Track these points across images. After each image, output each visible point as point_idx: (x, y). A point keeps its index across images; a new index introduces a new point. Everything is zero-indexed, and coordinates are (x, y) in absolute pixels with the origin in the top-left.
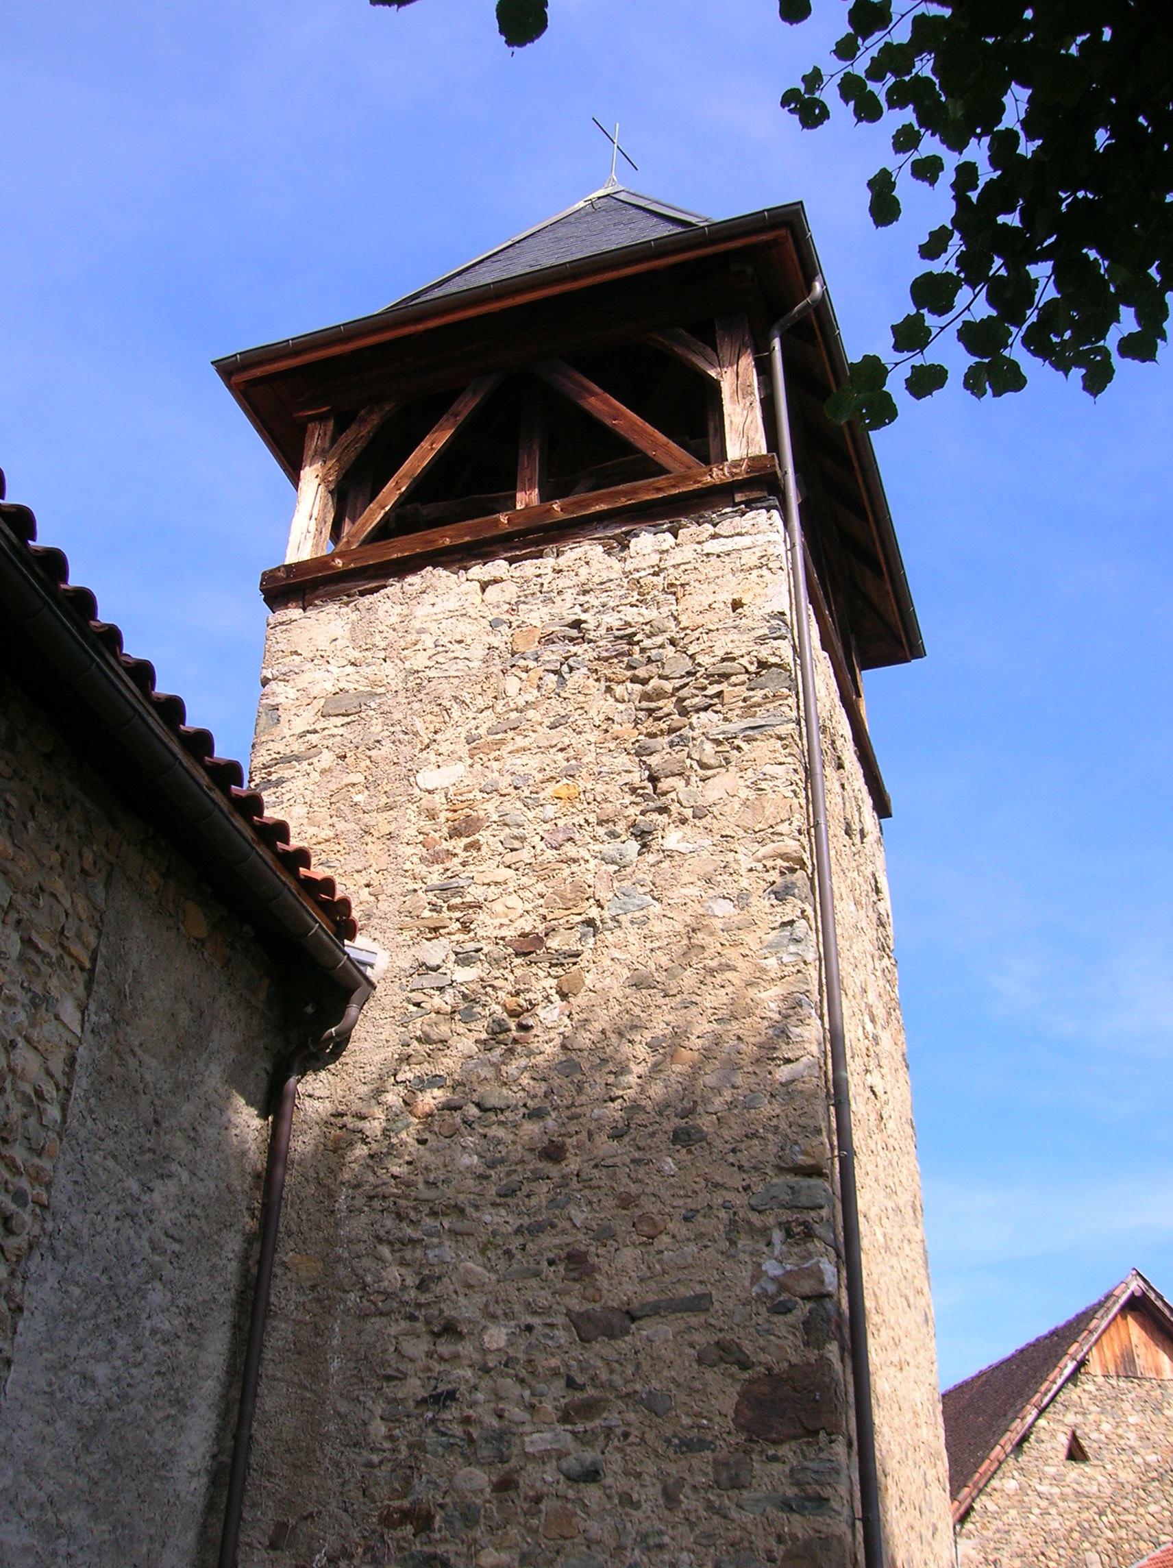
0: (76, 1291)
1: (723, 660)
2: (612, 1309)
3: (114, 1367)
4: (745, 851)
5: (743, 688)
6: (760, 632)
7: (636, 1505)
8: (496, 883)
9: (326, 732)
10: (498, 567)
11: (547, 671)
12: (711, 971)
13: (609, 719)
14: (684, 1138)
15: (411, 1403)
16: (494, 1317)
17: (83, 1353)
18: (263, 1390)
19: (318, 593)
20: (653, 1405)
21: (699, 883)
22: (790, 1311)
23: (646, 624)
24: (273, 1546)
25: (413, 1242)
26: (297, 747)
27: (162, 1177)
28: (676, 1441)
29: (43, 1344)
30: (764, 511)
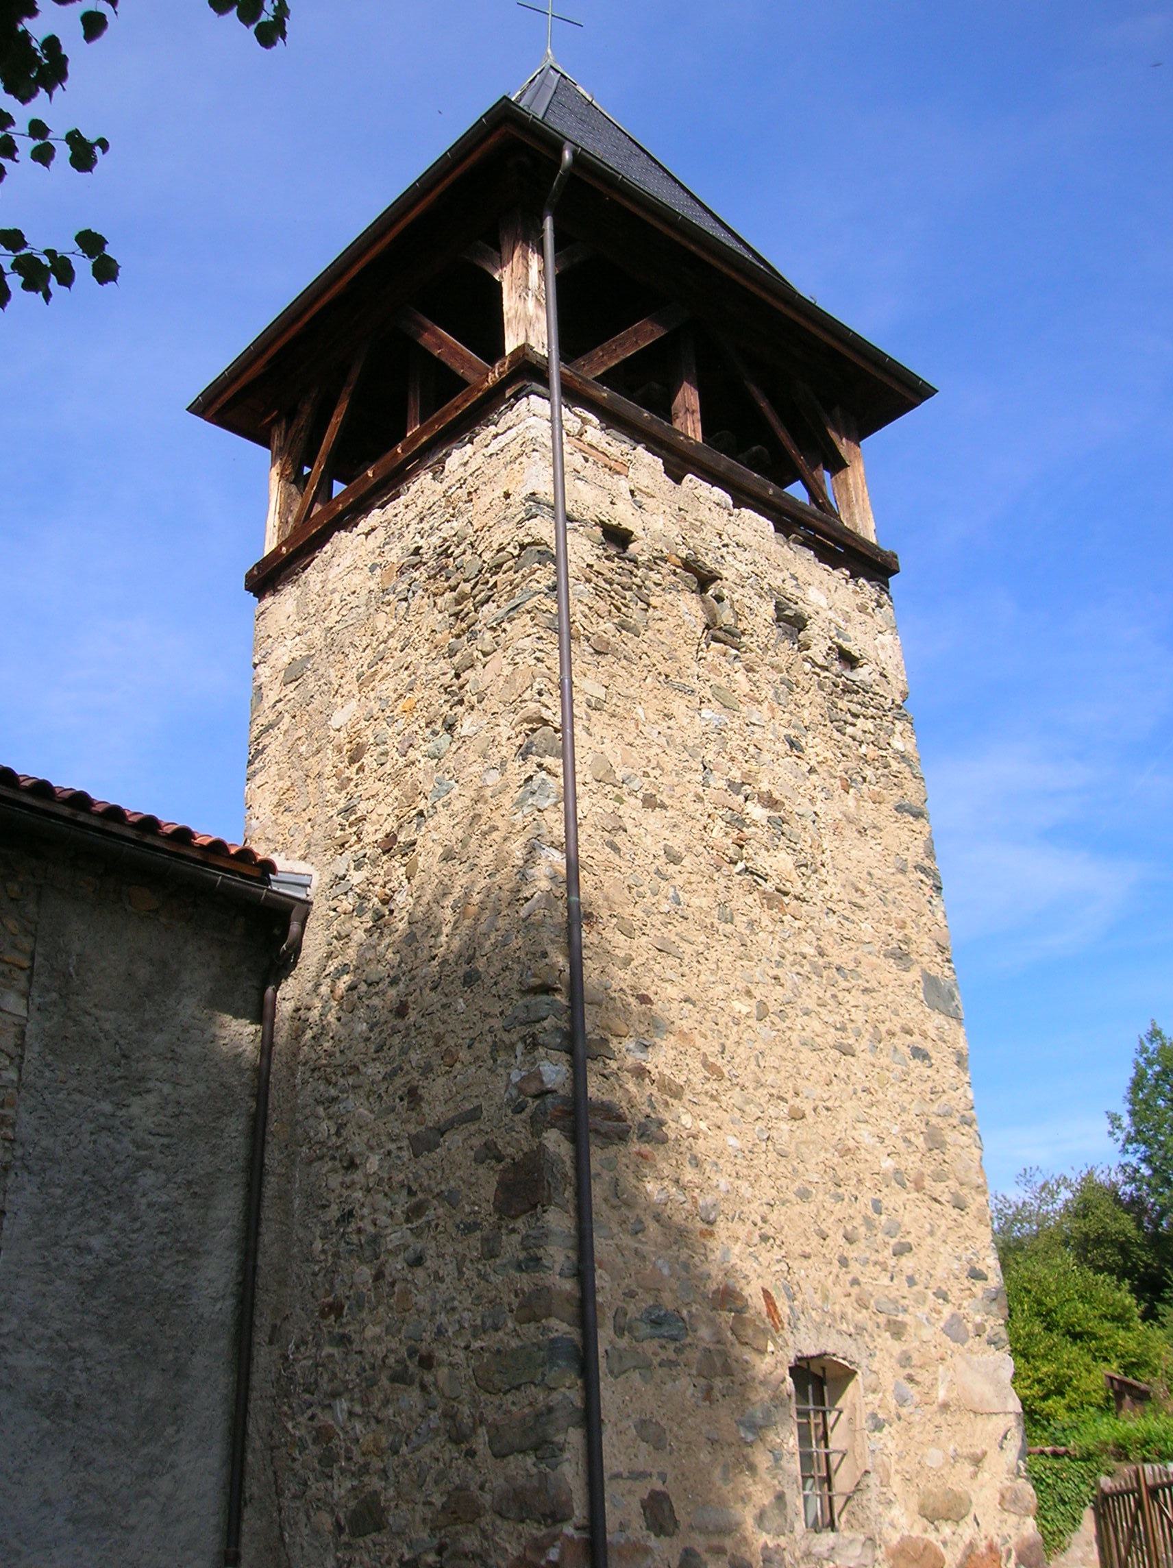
0: (59, 1191)
1: (498, 551)
2: (431, 1129)
3: (111, 1236)
4: (506, 723)
5: (511, 572)
6: (519, 518)
7: (442, 1280)
8: (373, 796)
9: (287, 698)
10: (375, 516)
11: (400, 600)
12: (484, 834)
13: (433, 631)
14: (470, 979)
15: (333, 1223)
16: (371, 1148)
17: (73, 1231)
18: (263, 1230)
19: (282, 577)
20: (451, 1199)
21: (479, 760)
22: (523, 1110)
23: (454, 536)
24: (271, 1342)
25: (334, 1100)
26: (272, 717)
27: (139, 1094)
28: (462, 1226)
29: (31, 1232)
30: (525, 399)
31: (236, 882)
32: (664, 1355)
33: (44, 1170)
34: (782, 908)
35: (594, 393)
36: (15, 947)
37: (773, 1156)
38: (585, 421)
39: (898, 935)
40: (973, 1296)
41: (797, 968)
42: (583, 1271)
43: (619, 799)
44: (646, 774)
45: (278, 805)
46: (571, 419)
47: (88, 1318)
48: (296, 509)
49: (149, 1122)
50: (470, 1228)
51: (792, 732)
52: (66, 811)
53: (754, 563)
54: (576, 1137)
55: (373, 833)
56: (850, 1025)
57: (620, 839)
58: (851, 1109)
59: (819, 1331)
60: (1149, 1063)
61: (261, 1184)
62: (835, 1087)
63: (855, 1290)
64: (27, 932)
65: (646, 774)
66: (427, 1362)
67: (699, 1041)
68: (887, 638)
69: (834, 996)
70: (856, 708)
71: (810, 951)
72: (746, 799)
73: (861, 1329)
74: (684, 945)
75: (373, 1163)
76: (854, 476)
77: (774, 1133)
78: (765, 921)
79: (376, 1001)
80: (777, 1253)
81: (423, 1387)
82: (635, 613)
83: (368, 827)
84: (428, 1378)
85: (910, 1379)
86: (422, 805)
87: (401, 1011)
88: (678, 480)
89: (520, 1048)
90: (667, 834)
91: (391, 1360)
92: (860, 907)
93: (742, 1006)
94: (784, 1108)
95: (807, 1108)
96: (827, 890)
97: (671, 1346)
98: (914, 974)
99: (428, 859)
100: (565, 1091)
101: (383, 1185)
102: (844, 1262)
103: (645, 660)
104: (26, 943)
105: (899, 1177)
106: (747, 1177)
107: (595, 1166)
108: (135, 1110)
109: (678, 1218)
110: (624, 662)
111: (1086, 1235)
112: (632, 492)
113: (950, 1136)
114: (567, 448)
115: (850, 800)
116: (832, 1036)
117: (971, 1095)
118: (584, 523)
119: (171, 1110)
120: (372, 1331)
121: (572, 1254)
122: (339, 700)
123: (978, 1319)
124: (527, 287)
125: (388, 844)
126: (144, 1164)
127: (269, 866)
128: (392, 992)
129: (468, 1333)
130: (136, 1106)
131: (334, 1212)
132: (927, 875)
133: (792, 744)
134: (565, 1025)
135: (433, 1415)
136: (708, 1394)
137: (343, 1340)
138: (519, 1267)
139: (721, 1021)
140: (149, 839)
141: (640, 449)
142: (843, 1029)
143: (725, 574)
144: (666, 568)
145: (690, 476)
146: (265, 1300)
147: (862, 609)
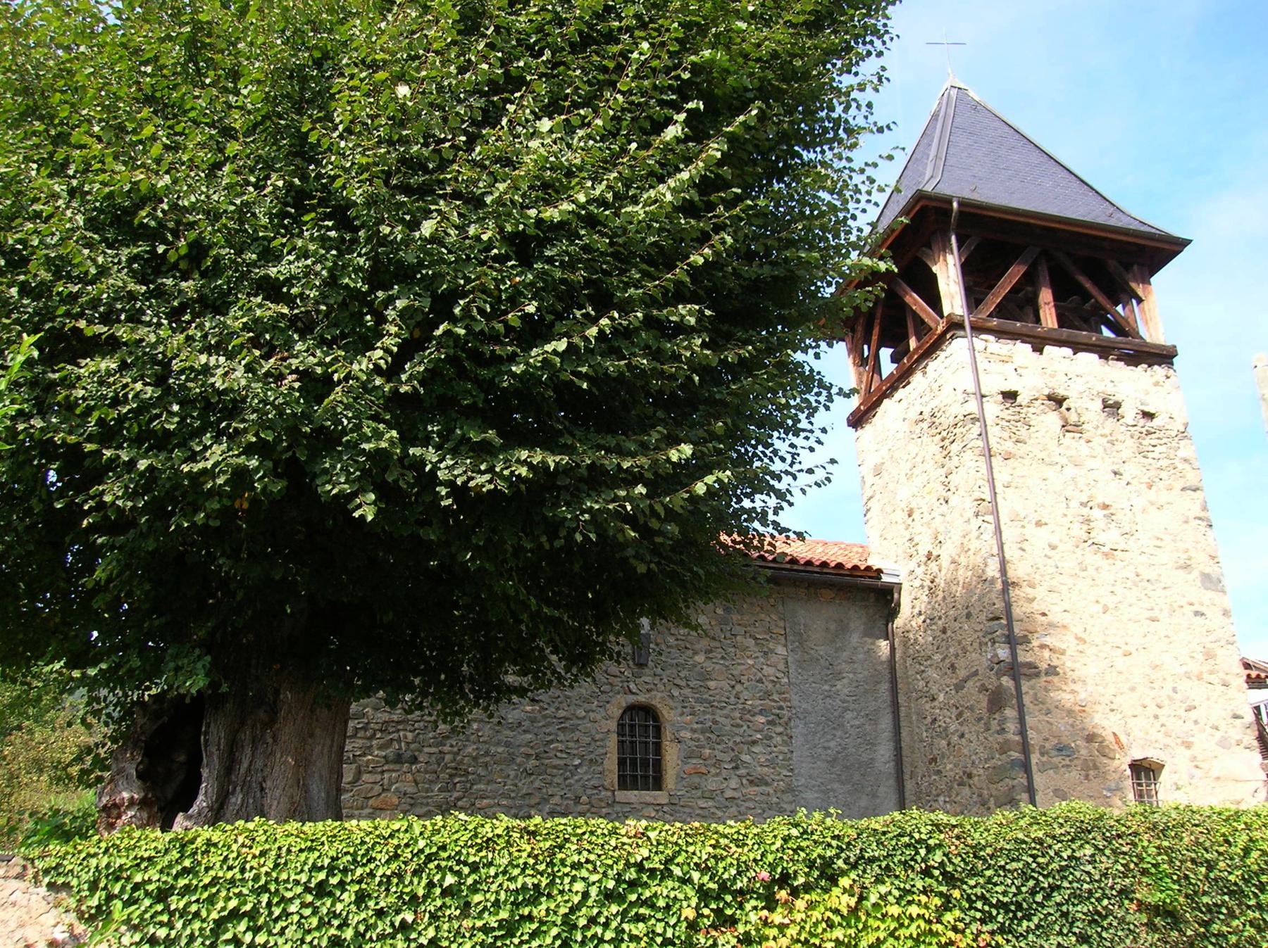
10: (900, 393)
20: (971, 708)
31: (868, 581)
34: (1114, 557)
39: (1185, 556)
42: (1023, 732)
43: (1023, 527)
46: (979, 343)
49: (846, 691)
50: (980, 719)
52: (788, 566)
54: (1016, 679)
55: (923, 551)
57: (1025, 545)
63: (1163, 729)
64: (781, 619)
66: (970, 776)
70: (1153, 442)
73: (1167, 746)
75: (941, 697)
79: (934, 627)
80: (1119, 716)
82: (1023, 433)
87: (944, 631)
95: (1132, 649)
99: (945, 561)
104: (781, 624)
107: (1024, 689)
108: (839, 687)
109: (1068, 705)
113: (1219, 652)
118: (992, 396)
119: (854, 684)
120: (950, 766)
123: (1239, 737)
125: (929, 556)
126: (847, 709)
127: (879, 571)
128: (940, 623)
131: (929, 719)
133: (1115, 473)
136: (1087, 777)
137: (939, 772)
147: (1157, 384)
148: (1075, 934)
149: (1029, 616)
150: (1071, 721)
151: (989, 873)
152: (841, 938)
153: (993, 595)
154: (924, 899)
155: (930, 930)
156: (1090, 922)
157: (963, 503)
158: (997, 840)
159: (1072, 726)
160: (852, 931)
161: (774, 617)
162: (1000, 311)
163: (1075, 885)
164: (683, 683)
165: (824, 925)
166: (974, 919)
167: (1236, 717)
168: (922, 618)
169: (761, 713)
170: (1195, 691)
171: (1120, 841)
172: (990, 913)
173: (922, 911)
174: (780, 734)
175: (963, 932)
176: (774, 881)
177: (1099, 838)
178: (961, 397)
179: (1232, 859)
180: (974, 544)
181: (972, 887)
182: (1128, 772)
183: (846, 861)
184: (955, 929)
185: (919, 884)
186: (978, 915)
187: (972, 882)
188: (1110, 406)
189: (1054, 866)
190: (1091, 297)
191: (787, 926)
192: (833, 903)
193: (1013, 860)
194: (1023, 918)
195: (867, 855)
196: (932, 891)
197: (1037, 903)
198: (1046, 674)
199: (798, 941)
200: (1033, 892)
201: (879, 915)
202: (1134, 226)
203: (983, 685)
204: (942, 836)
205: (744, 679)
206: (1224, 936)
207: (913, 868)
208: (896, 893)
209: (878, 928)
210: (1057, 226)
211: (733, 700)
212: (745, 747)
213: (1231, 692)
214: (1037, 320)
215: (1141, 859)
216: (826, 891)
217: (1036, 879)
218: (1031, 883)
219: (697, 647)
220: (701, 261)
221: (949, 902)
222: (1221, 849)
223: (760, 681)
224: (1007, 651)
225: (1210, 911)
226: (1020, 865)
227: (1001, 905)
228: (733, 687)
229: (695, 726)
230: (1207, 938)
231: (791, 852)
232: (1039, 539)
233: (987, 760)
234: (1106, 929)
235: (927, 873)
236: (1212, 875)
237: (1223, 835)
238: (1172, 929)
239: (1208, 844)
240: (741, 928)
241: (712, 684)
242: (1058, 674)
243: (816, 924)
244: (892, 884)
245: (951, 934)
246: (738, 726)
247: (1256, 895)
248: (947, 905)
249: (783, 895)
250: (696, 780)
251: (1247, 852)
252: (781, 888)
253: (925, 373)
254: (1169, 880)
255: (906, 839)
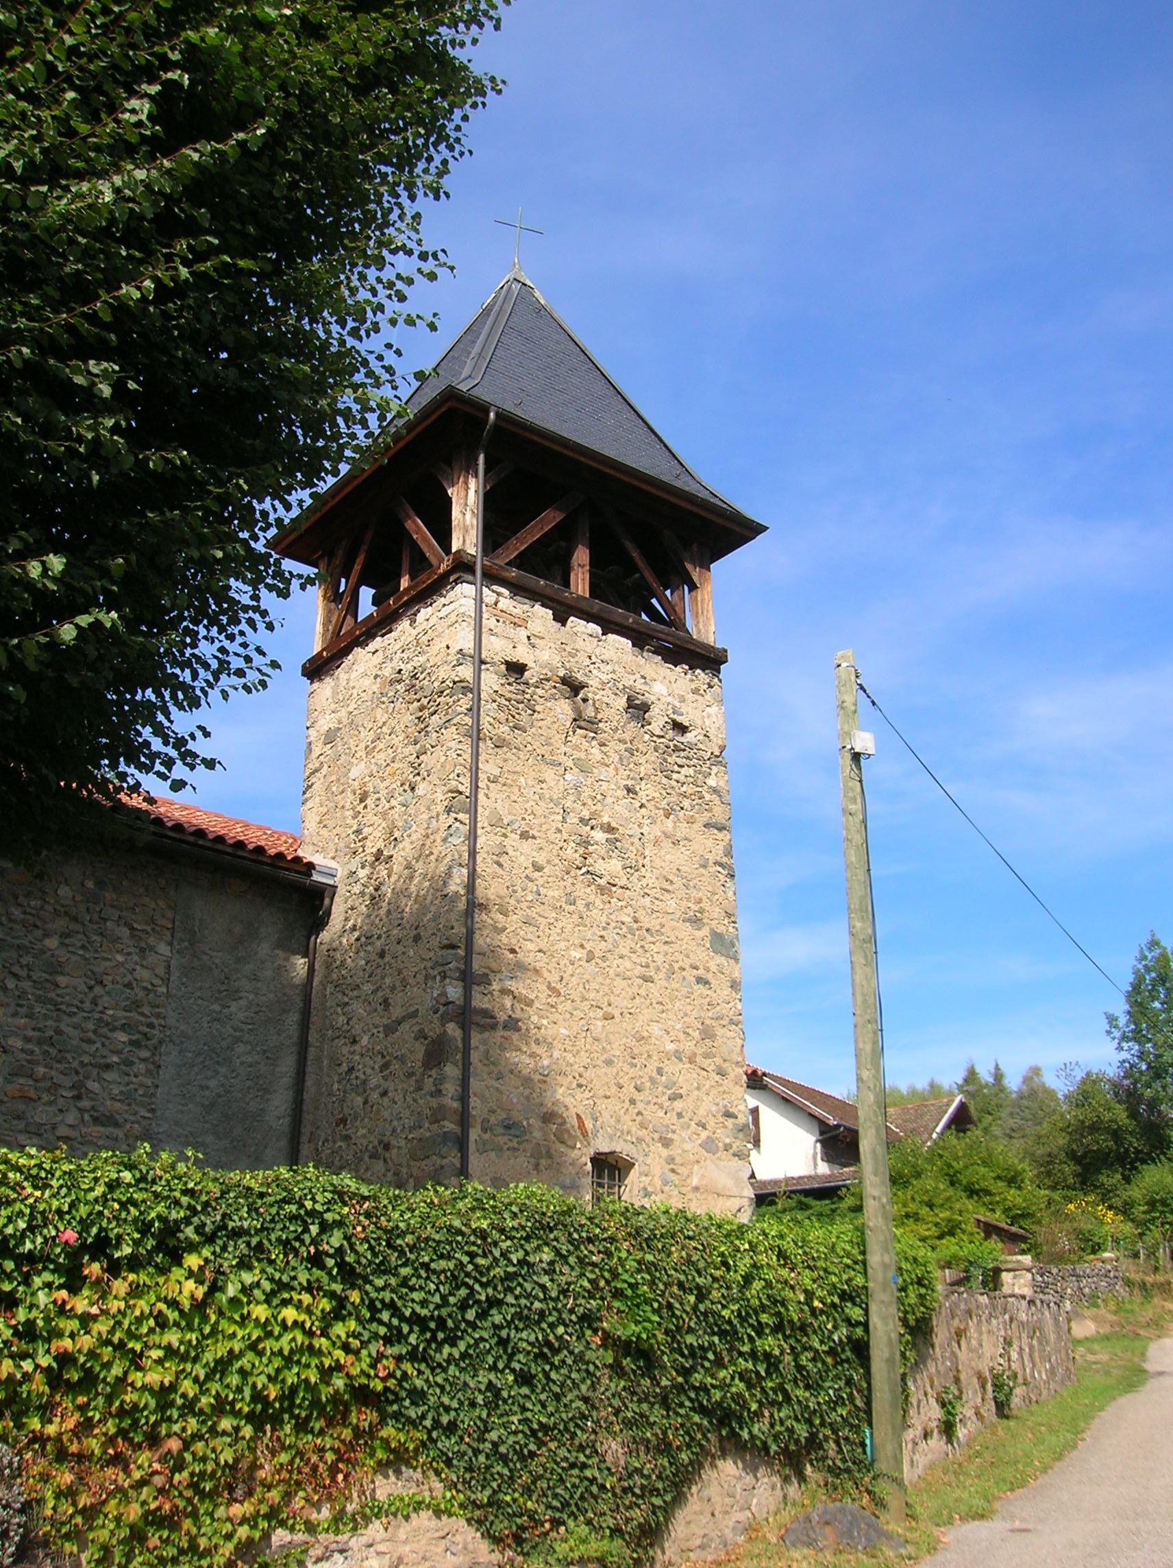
10: (377, 642)
18: (307, 1078)
20: (402, 1059)
25: (347, 1004)
31: (293, 876)
32: (510, 1144)
33: (182, 1043)
35: (506, 574)
36: (163, 916)
37: (589, 1040)
38: (499, 594)
40: (725, 1127)
41: (618, 930)
42: (464, 1098)
43: (505, 836)
44: (524, 819)
45: (320, 822)
46: (488, 595)
47: (207, 1126)
48: (334, 620)
49: (241, 1016)
50: (411, 1075)
51: (629, 783)
53: (614, 672)
54: (465, 1027)
55: (371, 848)
56: (652, 965)
58: (647, 1013)
59: (612, 1140)
60: (1146, 968)
61: (306, 1052)
62: (637, 1001)
63: (640, 1118)
64: (170, 907)
65: (524, 819)
66: (387, 1147)
67: (546, 974)
68: (714, 709)
69: (642, 947)
70: (680, 761)
71: (627, 919)
72: (592, 828)
74: (541, 919)
75: (365, 1040)
76: (703, 595)
77: (592, 1027)
78: (598, 903)
79: (369, 948)
81: (385, 1160)
82: (524, 718)
83: (368, 844)
84: (387, 1155)
85: (673, 1171)
86: (397, 834)
87: (382, 955)
88: (564, 624)
89: (438, 978)
90: (535, 854)
91: (370, 1147)
92: (668, 891)
93: (576, 954)
94: (600, 1013)
95: (616, 1013)
96: (644, 882)
97: (516, 1140)
98: (705, 931)
100: (460, 1002)
101: (369, 1052)
102: (633, 1102)
103: (529, 747)
104: (170, 914)
105: (678, 1055)
106: (571, 1051)
107: (474, 1042)
108: (233, 1009)
109: (526, 1072)
110: (514, 751)
111: (1083, 1122)
112: (529, 638)
113: (720, 1032)
114: (485, 616)
115: (669, 823)
116: (638, 970)
117: (739, 1007)
118: (493, 664)
119: (254, 1009)
120: (362, 1132)
121: (459, 1089)
122: (354, 760)
123: (728, 1141)
124: (466, 505)
125: (378, 855)
126: (238, 1040)
127: (311, 866)
128: (378, 943)
129: (407, 1130)
130: (234, 1007)
131: (345, 1067)
132: (724, 868)
133: (629, 791)
134: (463, 967)
135: (389, 1174)
137: (347, 1138)
138: (432, 1096)
139: (562, 963)
140: (240, 853)
141: (537, 607)
142: (647, 966)
143: (590, 682)
144: (548, 685)
145: (572, 618)
146: (307, 1118)
147: (696, 691)
148: (513, 1371)
149: (493, 951)
150: (527, 1092)
151: (405, 1271)
152: (176, 1344)
153: (453, 916)
154: (306, 1298)
155: (311, 1347)
156: (536, 1356)
157: (432, 792)
158: (423, 1226)
159: (528, 1098)
160: (193, 1337)
161: (161, 903)
162: (521, 562)
163: (523, 1301)
164: (23, 973)
165: (152, 1322)
166: (376, 1336)
167: (728, 1115)
168: (356, 934)
169: (123, 1028)
170: (684, 1076)
171: (591, 1247)
172: (399, 1330)
173: (302, 1317)
174: (144, 1060)
175: (357, 1353)
176: (84, 1248)
177: (563, 1239)
178: (453, 659)
179: (729, 1288)
180: (438, 849)
181: (378, 1290)
182: (589, 1166)
183: (199, 1230)
184: (346, 1348)
185: (303, 1277)
186: (382, 1330)
187: (379, 1282)
188: (636, 707)
189: (498, 1271)
190: (637, 570)
191: (95, 1318)
192: (171, 1291)
193: (442, 1257)
194: (445, 1341)
195: (231, 1224)
196: (320, 1288)
197: (468, 1323)
198: (504, 1028)
199: (108, 1342)
200: (463, 1306)
201: (237, 1317)
202: (703, 494)
203: (421, 1031)
204: (346, 1209)
205: (107, 980)
206: (707, 1391)
207: (296, 1252)
208: (267, 1286)
209: (234, 1335)
210: (612, 472)
211: (87, 1005)
212: (95, 1072)
213: (727, 1083)
214: (567, 584)
215: (615, 1275)
216: (163, 1271)
217: (471, 1288)
218: (463, 1292)
219: (49, 926)
220: (136, 295)
221: (344, 1307)
222: (718, 1273)
223: (128, 985)
224: (460, 990)
225: (693, 1354)
226: (451, 1265)
227: (416, 1320)
228: (91, 988)
229: (30, 1033)
230: (685, 1392)
231: (116, 1206)
232: (523, 853)
233: (412, 1129)
234: (557, 1369)
235: (316, 1261)
236: (702, 1307)
237: (722, 1255)
238: (643, 1376)
239: (701, 1264)
240: (22, 1314)
241: (62, 980)
242: (519, 1030)
243: (139, 1320)
244: (263, 1271)
245: (339, 1354)
246: (90, 1041)
247: (750, 1338)
248: (339, 1311)
249: (94, 1269)
250: (21, 1107)
251: (748, 1279)
252: (93, 1259)
253: (413, 622)
254: (648, 1308)
255: (293, 1208)
